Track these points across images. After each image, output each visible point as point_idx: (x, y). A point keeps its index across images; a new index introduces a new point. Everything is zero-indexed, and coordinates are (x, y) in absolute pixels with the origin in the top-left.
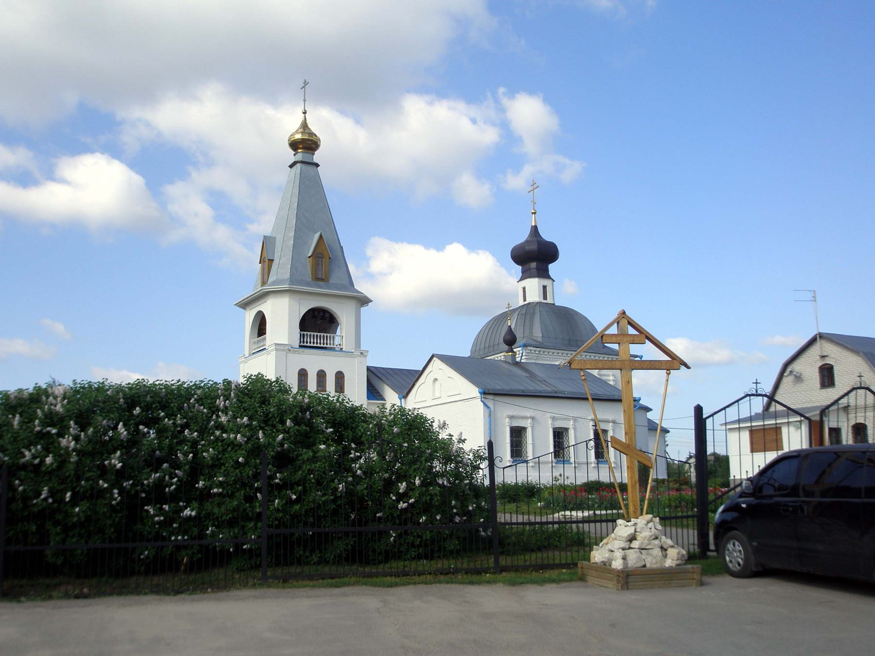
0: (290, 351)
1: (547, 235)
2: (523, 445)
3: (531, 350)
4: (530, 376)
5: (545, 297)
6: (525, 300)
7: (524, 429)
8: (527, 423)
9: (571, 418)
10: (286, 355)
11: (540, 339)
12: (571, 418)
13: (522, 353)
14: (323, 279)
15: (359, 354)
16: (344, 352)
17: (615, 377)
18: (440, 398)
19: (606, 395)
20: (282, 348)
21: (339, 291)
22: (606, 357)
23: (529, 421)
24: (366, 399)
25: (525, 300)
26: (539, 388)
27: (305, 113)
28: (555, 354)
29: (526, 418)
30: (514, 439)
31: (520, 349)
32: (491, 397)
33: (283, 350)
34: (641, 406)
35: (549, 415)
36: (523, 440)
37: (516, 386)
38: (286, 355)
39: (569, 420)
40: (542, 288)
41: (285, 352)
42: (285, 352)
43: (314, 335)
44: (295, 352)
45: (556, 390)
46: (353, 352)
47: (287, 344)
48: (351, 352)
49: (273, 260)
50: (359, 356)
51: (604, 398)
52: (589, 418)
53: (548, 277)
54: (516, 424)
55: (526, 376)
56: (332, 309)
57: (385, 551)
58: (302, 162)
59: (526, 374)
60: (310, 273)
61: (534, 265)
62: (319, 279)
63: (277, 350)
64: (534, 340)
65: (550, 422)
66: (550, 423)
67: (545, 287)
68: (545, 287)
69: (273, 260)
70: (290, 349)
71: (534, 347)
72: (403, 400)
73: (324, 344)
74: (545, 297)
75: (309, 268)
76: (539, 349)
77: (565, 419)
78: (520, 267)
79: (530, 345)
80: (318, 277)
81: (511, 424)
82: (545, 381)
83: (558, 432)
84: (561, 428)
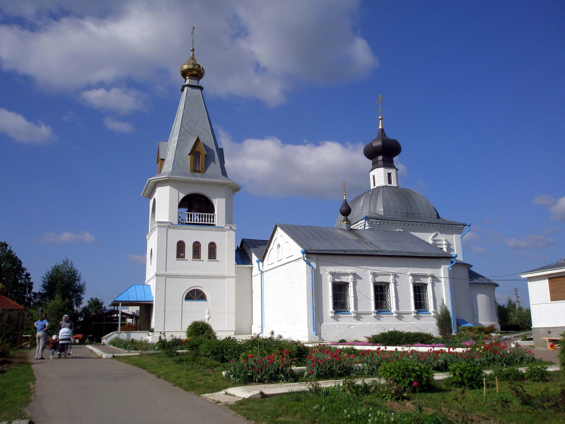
0: (170, 227)
1: (391, 135)
2: (387, 298)
3: (372, 222)
4: (359, 240)
5: (390, 182)
6: (374, 185)
7: (347, 284)
8: (349, 279)
9: (391, 273)
10: (167, 231)
11: (382, 213)
12: (391, 273)
13: (365, 224)
14: (200, 171)
15: (229, 228)
16: (216, 227)
17: (447, 242)
18: (282, 259)
19: (368, 249)
20: (163, 225)
21: (186, 177)
22: (374, 222)
23: (351, 277)
24: (234, 262)
25: (374, 185)
26: (362, 248)
27: (193, 50)
28: (418, 226)
29: (347, 274)
30: (417, 293)
31: (363, 221)
32: (314, 257)
33: (164, 227)
34: (457, 262)
35: (369, 272)
36: (387, 294)
37: (340, 247)
38: (167, 231)
39: (389, 275)
40: (387, 175)
41: (166, 228)
42: (166, 228)
43: (202, 215)
44: (174, 228)
45: (377, 249)
46: (223, 227)
47: (168, 221)
48: (222, 227)
49: (164, 159)
50: (228, 230)
51: (422, 255)
52: (408, 274)
53: (393, 167)
54: (379, 279)
55: (355, 240)
56: (205, 193)
57: (416, 393)
58: (188, 86)
59: (356, 238)
60: (189, 166)
61: (380, 158)
62: (196, 171)
63: (159, 226)
64: (377, 214)
65: (371, 277)
66: (371, 278)
67: (389, 175)
68: (389, 175)
69: (164, 159)
70: (169, 226)
71: (375, 219)
72: (261, 263)
73: (188, 221)
74: (390, 182)
75: (188, 163)
76: (379, 221)
77: (385, 275)
78: (371, 161)
79: (372, 217)
80: (195, 170)
81: (374, 280)
82: (370, 243)
83: (419, 287)
84: (382, 282)
